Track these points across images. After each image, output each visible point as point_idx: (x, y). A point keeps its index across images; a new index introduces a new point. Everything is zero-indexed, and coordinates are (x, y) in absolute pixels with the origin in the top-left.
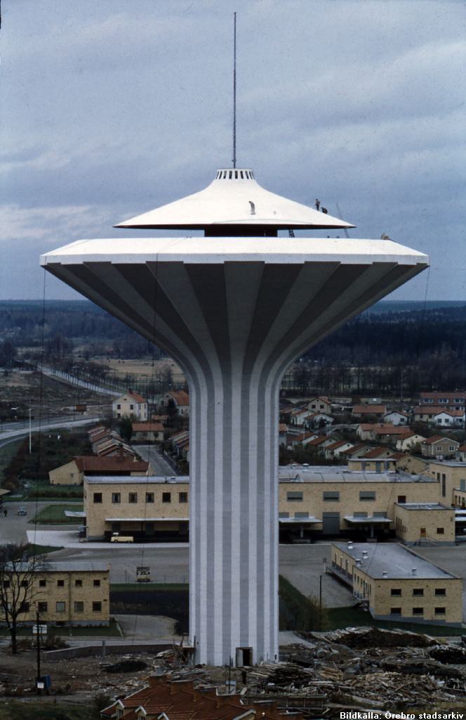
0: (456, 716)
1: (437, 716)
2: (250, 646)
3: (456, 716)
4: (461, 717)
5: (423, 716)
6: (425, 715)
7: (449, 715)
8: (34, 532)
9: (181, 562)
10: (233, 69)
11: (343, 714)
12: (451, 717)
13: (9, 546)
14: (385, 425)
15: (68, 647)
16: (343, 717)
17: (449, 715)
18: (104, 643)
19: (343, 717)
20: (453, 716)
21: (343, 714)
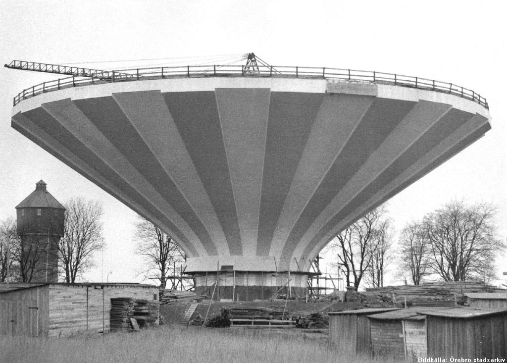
0: (500, 360)
1: (487, 361)
2: (244, 252)
3: (500, 360)
4: (504, 361)
5: (477, 360)
6: (478, 359)
7: (495, 360)
8: (249, 285)
9: (112, 320)
10: (220, 65)
11: (420, 359)
12: (496, 360)
13: (254, 286)
14: (178, 300)
15: (281, 287)
16: (420, 361)
17: (495, 360)
18: (351, 271)
19: (420, 361)
20: (498, 361)
21: (420, 359)
